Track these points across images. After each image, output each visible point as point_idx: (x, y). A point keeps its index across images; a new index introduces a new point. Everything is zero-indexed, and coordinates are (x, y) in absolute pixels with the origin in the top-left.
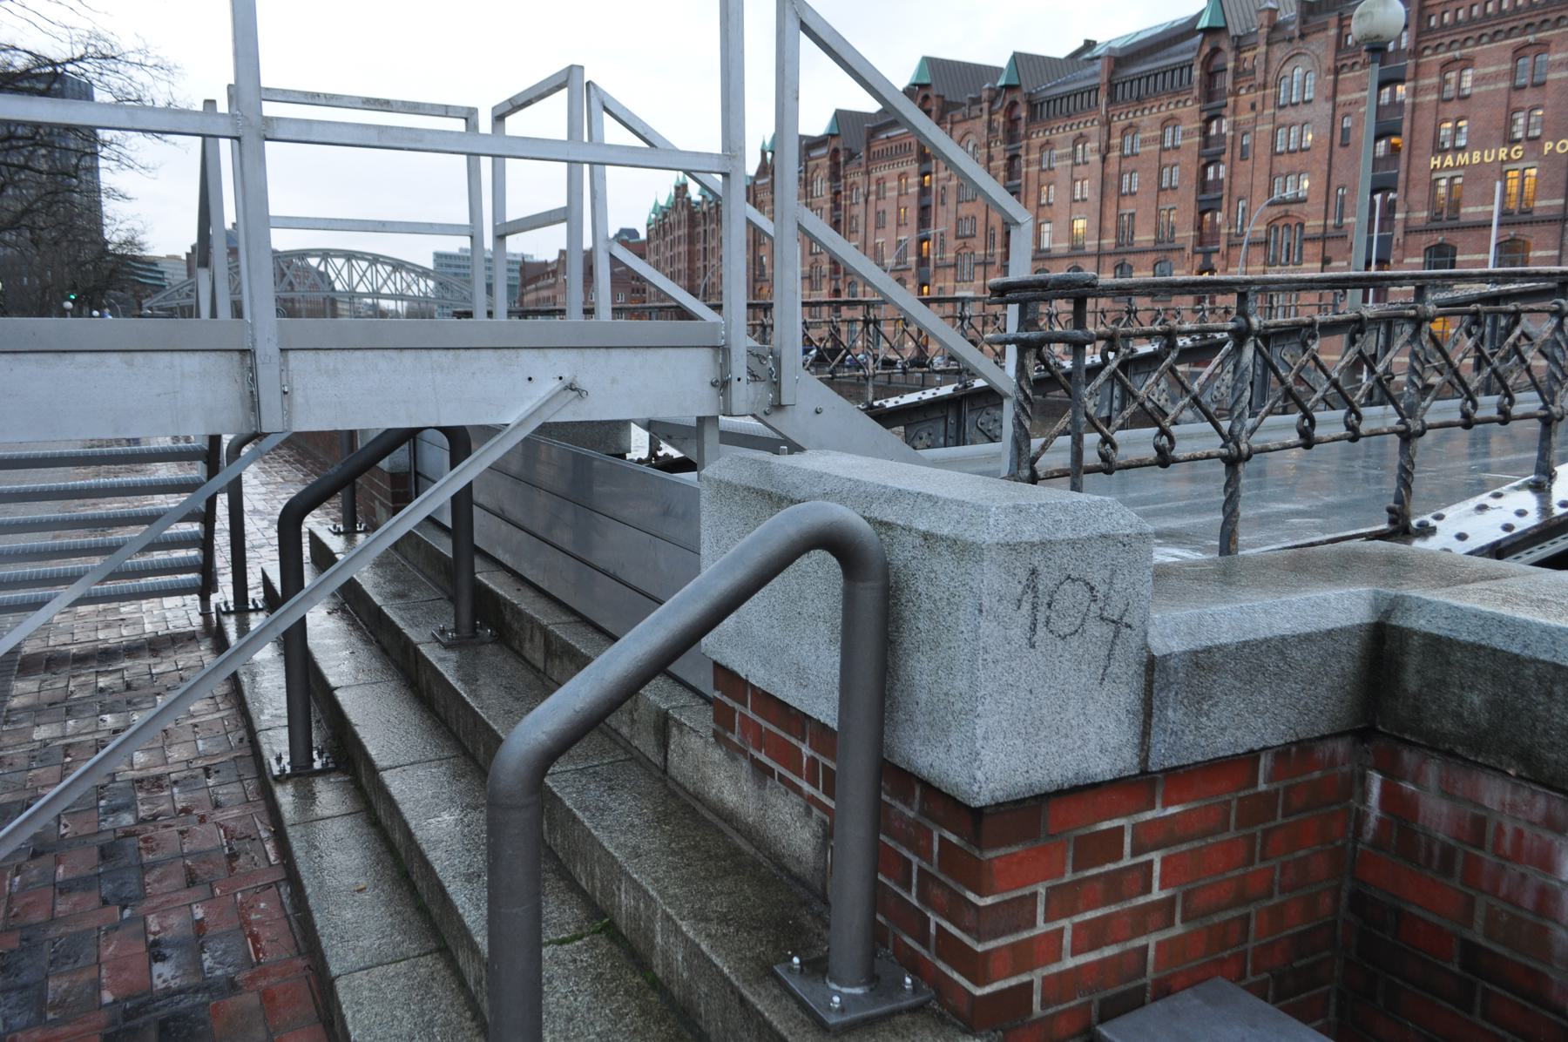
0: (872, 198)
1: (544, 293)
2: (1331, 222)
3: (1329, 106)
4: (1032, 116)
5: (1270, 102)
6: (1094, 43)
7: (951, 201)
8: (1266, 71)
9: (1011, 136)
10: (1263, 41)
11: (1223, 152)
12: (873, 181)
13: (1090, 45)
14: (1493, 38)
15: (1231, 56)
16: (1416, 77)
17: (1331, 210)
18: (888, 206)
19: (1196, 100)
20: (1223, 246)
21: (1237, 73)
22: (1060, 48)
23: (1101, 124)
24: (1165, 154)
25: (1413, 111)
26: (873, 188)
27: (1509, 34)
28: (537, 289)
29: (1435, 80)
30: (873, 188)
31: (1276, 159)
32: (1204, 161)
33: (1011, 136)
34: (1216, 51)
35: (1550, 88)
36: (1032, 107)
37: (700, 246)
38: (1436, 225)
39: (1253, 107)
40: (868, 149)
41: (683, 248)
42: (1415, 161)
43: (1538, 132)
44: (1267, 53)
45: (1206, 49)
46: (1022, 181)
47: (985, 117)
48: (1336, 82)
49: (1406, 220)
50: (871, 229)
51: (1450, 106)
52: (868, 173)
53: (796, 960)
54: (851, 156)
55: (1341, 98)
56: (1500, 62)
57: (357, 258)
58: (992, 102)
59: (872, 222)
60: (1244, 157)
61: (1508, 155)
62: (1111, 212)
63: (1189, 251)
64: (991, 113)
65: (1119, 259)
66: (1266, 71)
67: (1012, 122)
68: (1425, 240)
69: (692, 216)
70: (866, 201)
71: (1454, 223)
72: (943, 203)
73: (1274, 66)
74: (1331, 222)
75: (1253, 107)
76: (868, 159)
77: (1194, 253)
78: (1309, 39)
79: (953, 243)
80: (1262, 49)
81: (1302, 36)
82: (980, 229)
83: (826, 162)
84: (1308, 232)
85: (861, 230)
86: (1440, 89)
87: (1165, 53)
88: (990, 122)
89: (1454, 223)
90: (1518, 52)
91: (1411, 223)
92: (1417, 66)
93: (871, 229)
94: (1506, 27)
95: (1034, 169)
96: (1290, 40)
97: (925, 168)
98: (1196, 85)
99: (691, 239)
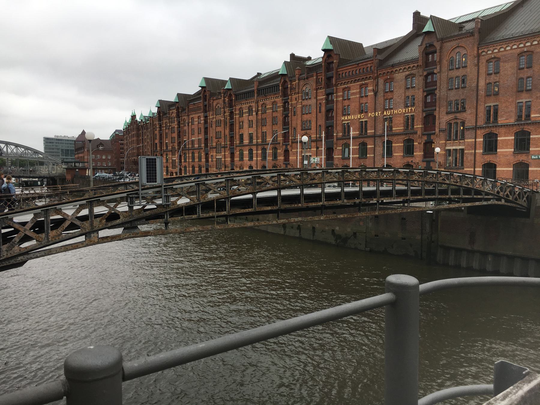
0: (190, 124)
1: (81, 155)
2: (318, 136)
3: (315, 100)
4: (236, 99)
5: (300, 98)
6: (261, 74)
7: (214, 126)
8: (299, 89)
9: (231, 106)
10: (297, 79)
11: (436, 89)
12: (190, 118)
13: (259, 74)
14: (354, 82)
15: (289, 83)
16: (336, 93)
17: (318, 132)
18: (195, 127)
19: (281, 97)
20: (290, 143)
21: (291, 89)
22: (247, 77)
23: (256, 103)
24: (274, 113)
25: (336, 103)
26: (190, 121)
27: (358, 81)
28: (78, 154)
29: (341, 94)
30: (190, 121)
31: (303, 116)
32: (425, 94)
33: (231, 106)
34: (285, 82)
35: (369, 97)
36: (236, 96)
37: (141, 138)
38: (344, 137)
39: (296, 99)
40: (188, 107)
41: (135, 139)
42: (338, 118)
43: (530, 88)
44: (298, 83)
45: (282, 81)
46: (234, 120)
47: (223, 99)
48: (317, 92)
49: (337, 136)
50: (190, 135)
51: (346, 101)
52: (188, 116)
53: (92, 347)
54: (184, 110)
55: (318, 98)
56: (357, 89)
57: (10, 145)
58: (224, 94)
59: (190, 132)
60: (294, 115)
61: (406, 111)
62: (260, 131)
63: (281, 144)
64: (224, 97)
65: (240, 148)
66: (299, 89)
67: (231, 100)
68: (341, 142)
69: (138, 129)
70: (188, 125)
71: (366, 136)
72: (212, 127)
73: (301, 87)
74: (318, 136)
75: (296, 99)
76: (188, 111)
77: (283, 145)
78: (309, 79)
79: (215, 140)
80: (297, 81)
81: (307, 78)
82: (223, 135)
83: (175, 111)
84: (215, 150)
85: (187, 135)
86: (343, 96)
87: (275, 80)
88: (224, 100)
89: (366, 136)
90: (407, 77)
91: (338, 137)
92: (337, 89)
93: (190, 135)
94: (357, 79)
95: (238, 116)
96: (304, 79)
97: (329, 90)
98: (280, 91)
99: (138, 136)
